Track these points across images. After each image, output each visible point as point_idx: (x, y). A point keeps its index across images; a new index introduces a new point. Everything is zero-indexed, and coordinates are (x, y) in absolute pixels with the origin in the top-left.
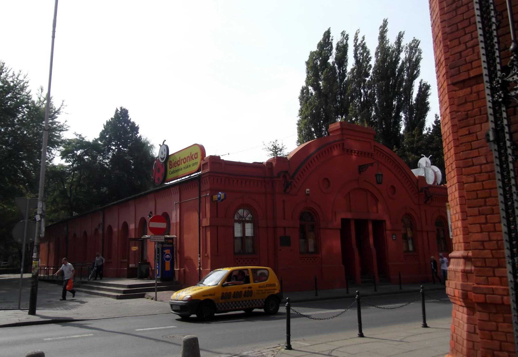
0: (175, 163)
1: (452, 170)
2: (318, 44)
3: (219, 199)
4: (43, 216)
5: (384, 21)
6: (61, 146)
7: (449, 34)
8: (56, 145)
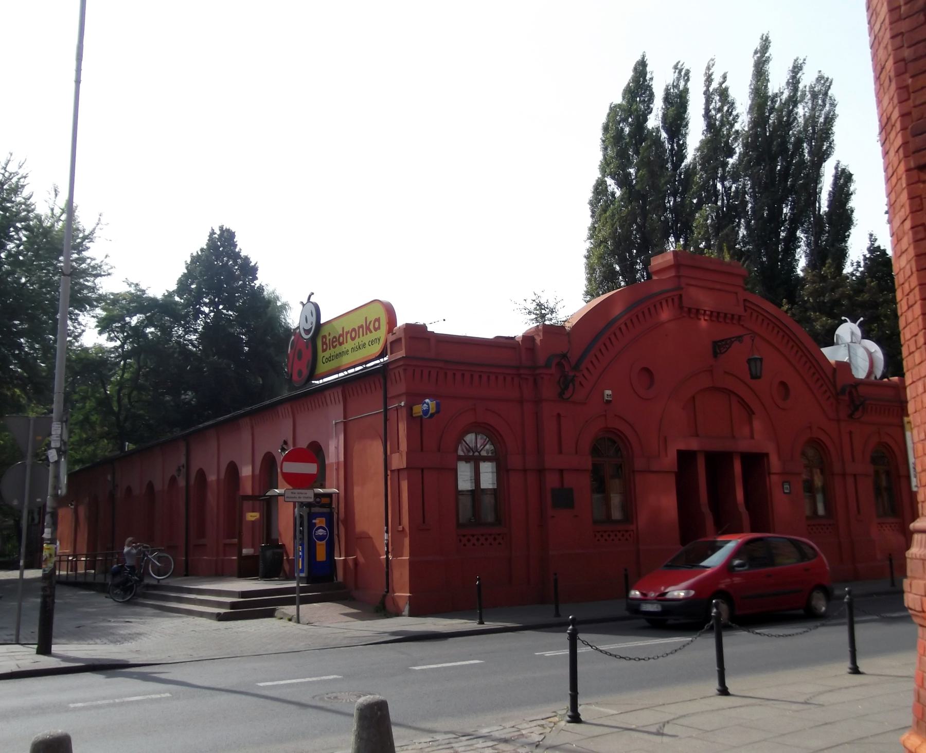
0: (334, 340)
1: (917, 349)
2: (624, 90)
3: (426, 412)
4: (63, 452)
5: (762, 38)
6: (97, 307)
7: (910, 61)
8: (87, 306)
